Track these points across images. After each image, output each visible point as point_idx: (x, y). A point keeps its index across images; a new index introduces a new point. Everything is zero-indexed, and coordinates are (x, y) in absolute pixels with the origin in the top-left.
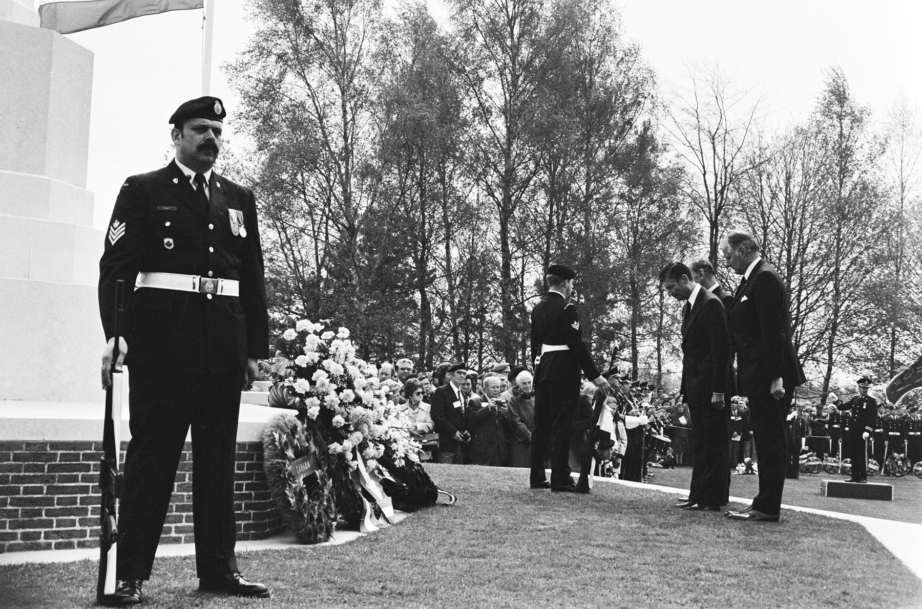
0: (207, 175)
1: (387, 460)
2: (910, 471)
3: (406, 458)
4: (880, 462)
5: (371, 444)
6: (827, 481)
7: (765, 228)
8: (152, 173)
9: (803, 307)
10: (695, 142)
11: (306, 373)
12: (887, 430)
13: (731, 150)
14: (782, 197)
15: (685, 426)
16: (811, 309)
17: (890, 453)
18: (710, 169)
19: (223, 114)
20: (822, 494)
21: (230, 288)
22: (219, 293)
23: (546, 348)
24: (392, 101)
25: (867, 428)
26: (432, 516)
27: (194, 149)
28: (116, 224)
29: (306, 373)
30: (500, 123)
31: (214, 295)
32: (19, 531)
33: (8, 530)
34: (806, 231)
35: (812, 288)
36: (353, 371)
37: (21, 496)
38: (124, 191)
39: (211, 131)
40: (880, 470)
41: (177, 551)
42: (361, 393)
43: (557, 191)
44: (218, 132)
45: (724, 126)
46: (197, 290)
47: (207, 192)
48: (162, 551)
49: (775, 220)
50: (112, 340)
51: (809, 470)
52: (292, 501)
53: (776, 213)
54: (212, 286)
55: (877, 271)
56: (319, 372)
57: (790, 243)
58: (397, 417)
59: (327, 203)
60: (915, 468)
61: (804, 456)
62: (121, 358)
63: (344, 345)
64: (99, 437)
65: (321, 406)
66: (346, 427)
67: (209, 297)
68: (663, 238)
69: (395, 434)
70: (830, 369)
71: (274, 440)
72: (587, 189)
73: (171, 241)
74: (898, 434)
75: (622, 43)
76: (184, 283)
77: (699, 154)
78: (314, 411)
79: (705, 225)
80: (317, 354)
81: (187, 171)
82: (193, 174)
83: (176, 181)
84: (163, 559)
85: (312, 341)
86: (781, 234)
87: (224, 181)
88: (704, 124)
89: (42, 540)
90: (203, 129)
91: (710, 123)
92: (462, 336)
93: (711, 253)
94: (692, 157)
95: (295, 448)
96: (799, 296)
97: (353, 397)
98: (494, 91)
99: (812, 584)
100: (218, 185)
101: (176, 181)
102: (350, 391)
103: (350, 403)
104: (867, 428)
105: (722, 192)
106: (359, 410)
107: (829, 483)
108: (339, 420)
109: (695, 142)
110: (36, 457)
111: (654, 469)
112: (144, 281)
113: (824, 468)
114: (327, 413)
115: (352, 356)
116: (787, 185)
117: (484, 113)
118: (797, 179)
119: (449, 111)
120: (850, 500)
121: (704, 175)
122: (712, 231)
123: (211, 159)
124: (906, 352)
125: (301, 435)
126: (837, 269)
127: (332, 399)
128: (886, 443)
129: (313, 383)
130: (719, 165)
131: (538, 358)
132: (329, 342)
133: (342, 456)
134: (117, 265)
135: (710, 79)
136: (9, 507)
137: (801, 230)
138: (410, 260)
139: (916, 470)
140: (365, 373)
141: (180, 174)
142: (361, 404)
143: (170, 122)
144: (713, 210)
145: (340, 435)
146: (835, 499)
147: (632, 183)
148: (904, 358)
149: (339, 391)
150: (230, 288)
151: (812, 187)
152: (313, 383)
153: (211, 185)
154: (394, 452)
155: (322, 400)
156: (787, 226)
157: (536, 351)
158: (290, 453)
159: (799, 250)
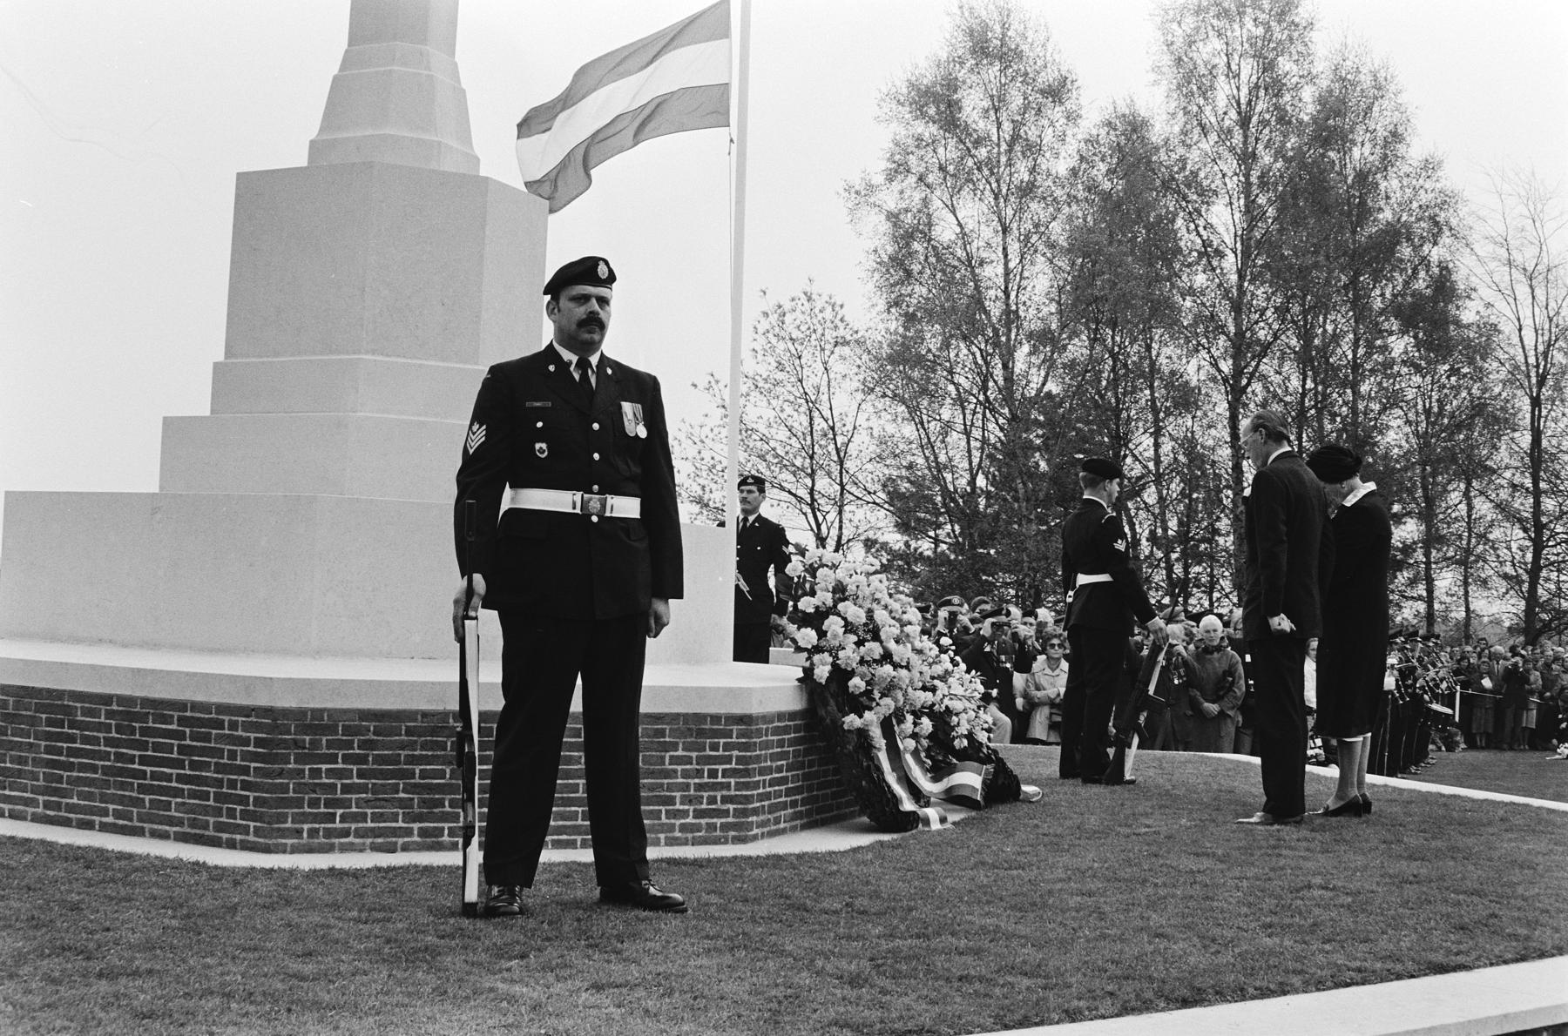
0: (594, 360)
3: (970, 736)
8: (523, 360)
15: (1491, 691)
18: (1527, 322)
19: (612, 278)
21: (627, 507)
22: (608, 514)
23: (1083, 579)
24: (1081, 246)
26: (1288, 832)
27: (574, 327)
31: (601, 517)
32: (416, 826)
33: (401, 824)
37: (417, 780)
38: (487, 384)
39: (594, 301)
41: (566, 854)
42: (892, 645)
43: (1311, 359)
44: (603, 301)
46: (578, 511)
47: (593, 380)
48: (548, 856)
54: (598, 505)
59: (985, 388)
62: (476, 601)
64: (455, 706)
65: (834, 665)
66: (868, 693)
67: (595, 519)
69: (957, 705)
73: (544, 446)
75: (1414, 151)
76: (560, 501)
77: (1511, 300)
78: (822, 672)
79: (1525, 404)
81: (568, 356)
82: (574, 359)
83: (552, 368)
84: (550, 866)
87: (617, 366)
88: (1518, 257)
89: (446, 838)
90: (585, 298)
91: (1526, 257)
92: (1178, 569)
94: (1501, 305)
98: (1223, 219)
100: (609, 371)
101: (552, 368)
103: (875, 661)
105: (1545, 354)
106: (887, 669)
108: (857, 684)
110: (434, 731)
111: (1436, 753)
112: (513, 500)
114: (841, 675)
117: (1209, 253)
119: (1162, 249)
123: (596, 337)
129: (822, 634)
130: (1541, 317)
131: (1071, 593)
133: (863, 733)
134: (479, 478)
135: (1523, 193)
136: (402, 795)
143: (545, 293)
144: (1534, 380)
145: (859, 704)
149: (859, 643)
150: (627, 507)
152: (822, 634)
154: (953, 729)
155: (836, 657)
157: (1068, 583)
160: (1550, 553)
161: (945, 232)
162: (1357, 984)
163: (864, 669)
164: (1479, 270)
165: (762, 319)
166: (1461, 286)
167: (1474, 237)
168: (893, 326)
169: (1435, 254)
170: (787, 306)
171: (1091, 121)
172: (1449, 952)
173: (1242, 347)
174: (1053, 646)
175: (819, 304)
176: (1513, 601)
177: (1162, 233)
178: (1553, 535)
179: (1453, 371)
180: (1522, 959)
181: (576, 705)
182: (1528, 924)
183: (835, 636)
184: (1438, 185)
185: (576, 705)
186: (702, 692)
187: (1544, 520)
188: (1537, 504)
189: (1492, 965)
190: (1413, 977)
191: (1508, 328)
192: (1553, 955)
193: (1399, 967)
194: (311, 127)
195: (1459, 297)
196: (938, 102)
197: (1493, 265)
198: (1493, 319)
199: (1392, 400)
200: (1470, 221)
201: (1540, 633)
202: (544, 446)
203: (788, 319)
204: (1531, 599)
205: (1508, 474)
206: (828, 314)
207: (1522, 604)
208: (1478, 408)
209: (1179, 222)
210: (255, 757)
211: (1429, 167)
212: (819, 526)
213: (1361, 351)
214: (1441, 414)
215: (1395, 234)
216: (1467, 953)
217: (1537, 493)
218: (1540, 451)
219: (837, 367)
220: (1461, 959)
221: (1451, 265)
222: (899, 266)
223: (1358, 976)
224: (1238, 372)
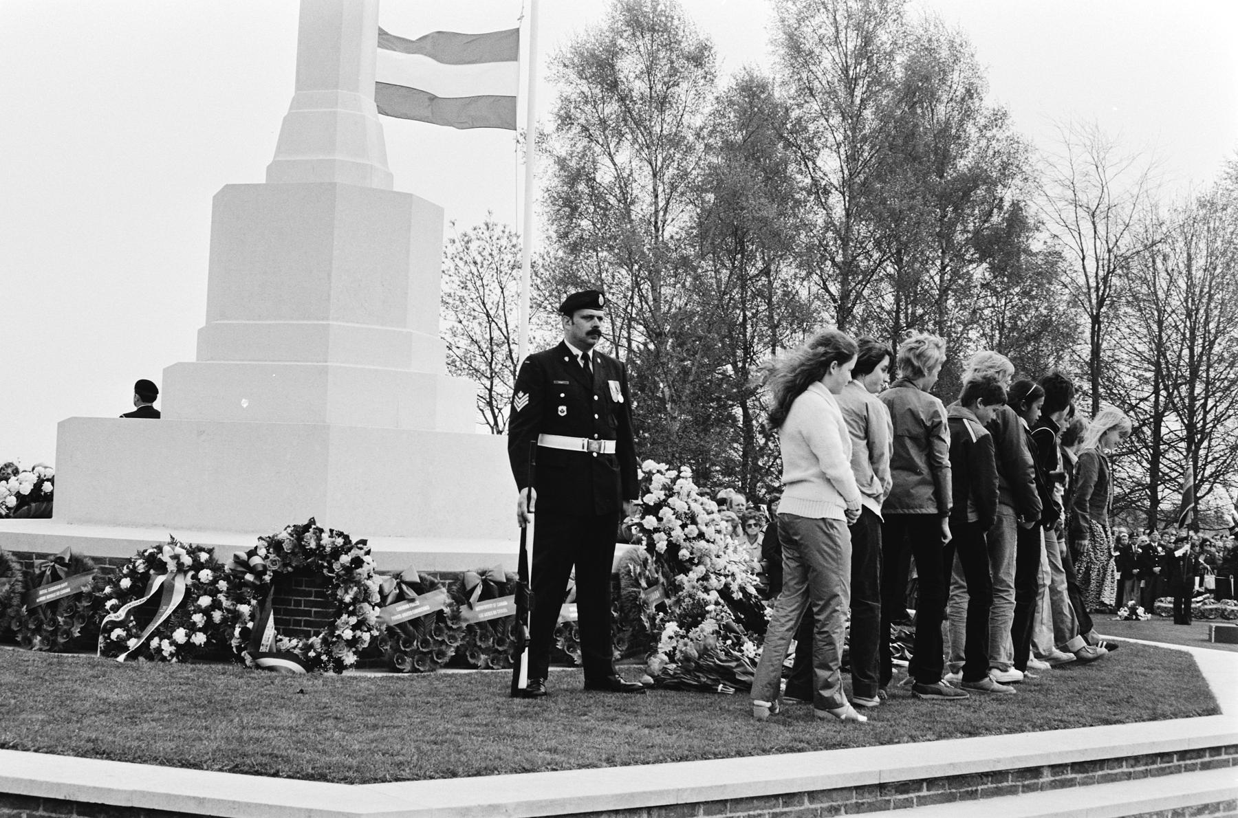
0: (590, 353)
1: (725, 592)
5: (713, 576)
6: (1214, 625)
7: (1160, 323)
9: (1210, 417)
10: (1071, 220)
11: (654, 510)
13: (1115, 230)
14: (1182, 283)
16: (1218, 420)
18: (1090, 253)
20: (1210, 640)
21: (610, 447)
27: (584, 335)
28: (521, 394)
29: (654, 510)
30: (837, 203)
34: (1212, 325)
36: (696, 507)
42: (704, 528)
43: (905, 285)
45: (1106, 200)
49: (1173, 311)
50: (525, 491)
51: (1203, 615)
52: (647, 625)
53: (1175, 301)
56: (665, 509)
57: (1193, 338)
58: (735, 551)
61: (1200, 598)
63: (686, 484)
68: (1036, 337)
69: (732, 568)
71: (629, 571)
72: (941, 281)
73: (564, 408)
75: (988, 102)
76: (574, 444)
78: (662, 546)
79: (1085, 321)
80: (663, 492)
81: (576, 351)
82: (580, 353)
83: (567, 359)
85: (658, 481)
86: (1181, 327)
90: (591, 317)
91: (1089, 197)
93: (1092, 351)
94: (1067, 238)
95: (647, 579)
96: (1204, 405)
97: (696, 532)
98: (830, 165)
102: (693, 527)
105: (1105, 279)
106: (703, 543)
109: (1071, 220)
114: (673, 548)
115: (694, 495)
116: (1189, 266)
117: (819, 191)
118: (1200, 262)
121: (1083, 260)
122: (1093, 328)
125: (651, 566)
127: (678, 534)
129: (660, 520)
132: (674, 481)
135: (1088, 143)
137: (1207, 323)
138: (729, 367)
140: (704, 507)
141: (569, 353)
144: (1094, 301)
145: (685, 567)
147: (995, 270)
149: (684, 526)
150: (610, 447)
151: (1219, 270)
152: (660, 520)
153: (594, 361)
155: (669, 535)
156: (1189, 316)
158: (644, 584)
159: (1204, 347)
161: (605, 176)
163: (687, 544)
164: (1049, 209)
165: (449, 245)
166: (1031, 221)
167: (1044, 180)
168: (561, 254)
169: (1008, 195)
170: (472, 234)
171: (725, 83)
173: (847, 270)
174: (750, 526)
175: (497, 232)
177: (775, 174)
179: (1025, 293)
183: (670, 521)
184: (1008, 134)
186: (435, 556)
191: (1071, 255)
194: (268, 156)
195: (1029, 230)
196: (599, 67)
197: (1061, 204)
198: (1058, 248)
199: (975, 317)
200: (1040, 166)
202: (564, 408)
203: (473, 246)
206: (504, 242)
208: (1045, 324)
209: (792, 167)
210: (315, 604)
211: (998, 118)
212: (495, 418)
213: (947, 277)
214: (1014, 327)
215: (976, 178)
218: (1099, 362)
219: (511, 287)
221: (1022, 204)
222: (568, 206)
224: (845, 295)
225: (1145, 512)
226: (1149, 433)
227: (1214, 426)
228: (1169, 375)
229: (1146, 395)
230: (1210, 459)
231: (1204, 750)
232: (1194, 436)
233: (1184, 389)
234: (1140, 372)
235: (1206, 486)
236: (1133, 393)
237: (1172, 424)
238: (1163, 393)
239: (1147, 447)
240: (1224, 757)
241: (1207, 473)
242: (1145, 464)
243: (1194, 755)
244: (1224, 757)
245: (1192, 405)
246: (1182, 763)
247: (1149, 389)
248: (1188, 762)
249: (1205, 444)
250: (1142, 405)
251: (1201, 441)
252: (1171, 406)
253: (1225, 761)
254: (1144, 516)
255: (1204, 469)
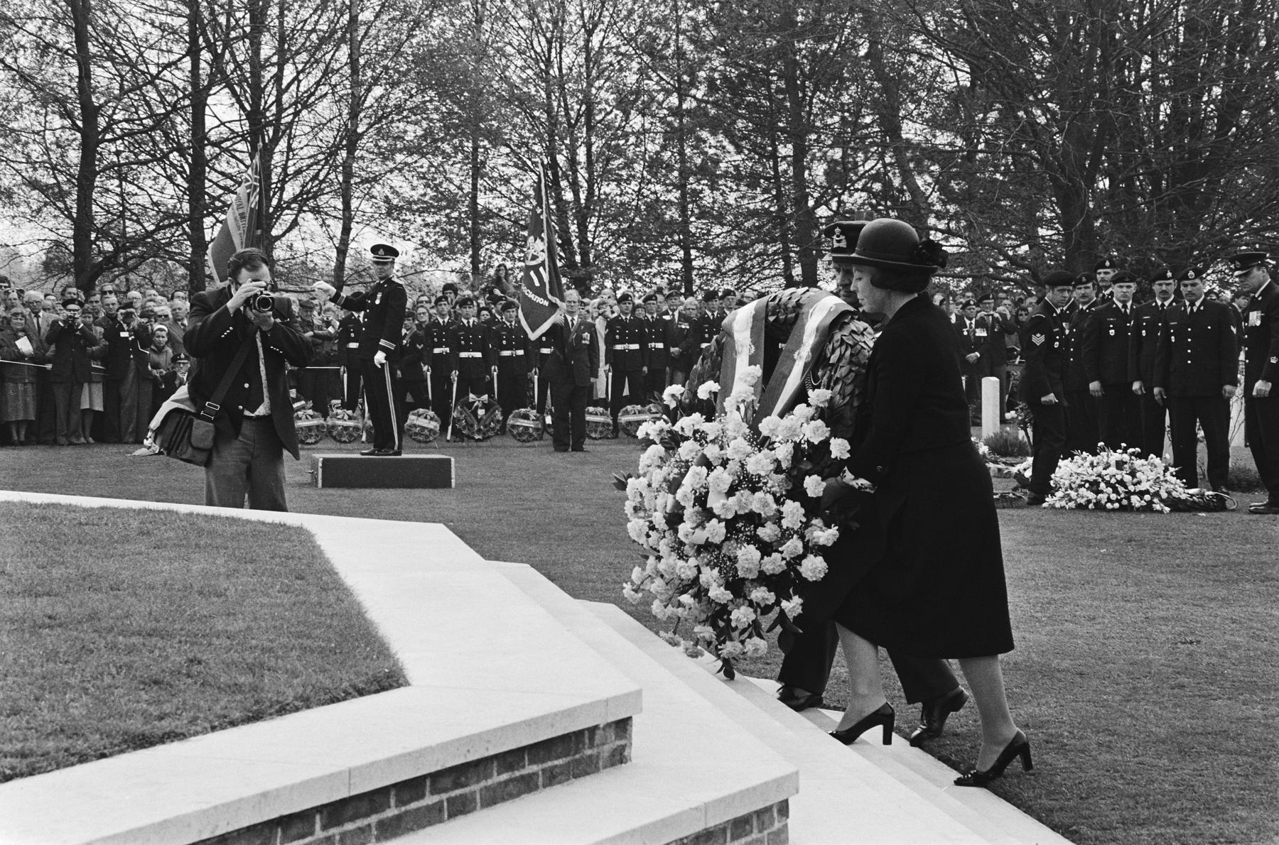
2: (503, 430)
4: (443, 415)
6: (320, 457)
12: (457, 348)
15: (32, 358)
16: (304, 103)
17: (462, 393)
20: (313, 484)
25: (383, 342)
35: (304, 56)
40: (443, 429)
55: (437, 23)
60: (510, 421)
70: (346, 230)
74: (479, 355)
96: (278, 78)
99: (131, 650)
104: (383, 342)
107: (325, 461)
113: (329, 433)
120: (368, 491)
124: (503, 189)
126: (353, 19)
128: (455, 375)
139: (513, 426)
142: (642, 503)
146: (331, 491)
148: (502, 203)
160: (108, 151)
162: (22, 775)
172: (146, 717)
176: (51, 223)
178: (112, 122)
180: (255, 717)
181: (1168, 422)
182: (251, 669)
185: (1168, 422)
187: (96, 100)
188: (85, 75)
189: (213, 729)
190: (103, 756)
192: (297, 709)
193: (80, 745)
201: (99, 270)
204: (83, 223)
205: (31, 26)
207: (66, 230)
216: (175, 714)
217: (84, 61)
220: (166, 725)
223: (22, 764)
225: (183, 264)
226: (183, 128)
227: (296, 114)
228: (215, 24)
229: (174, 57)
230: (291, 170)
231: (383, 792)
232: (261, 130)
233: (242, 50)
234: (163, 18)
235: (288, 217)
236: (151, 55)
237: (223, 110)
238: (206, 55)
239: (181, 150)
240: (430, 800)
241: (287, 196)
242: (179, 180)
243: (364, 806)
244: (430, 800)
245: (256, 75)
246: (334, 831)
247: (179, 49)
248: (349, 826)
249: (283, 144)
250: (166, 74)
251: (275, 140)
252: (219, 76)
253: (429, 808)
254: (182, 271)
255: (282, 189)
